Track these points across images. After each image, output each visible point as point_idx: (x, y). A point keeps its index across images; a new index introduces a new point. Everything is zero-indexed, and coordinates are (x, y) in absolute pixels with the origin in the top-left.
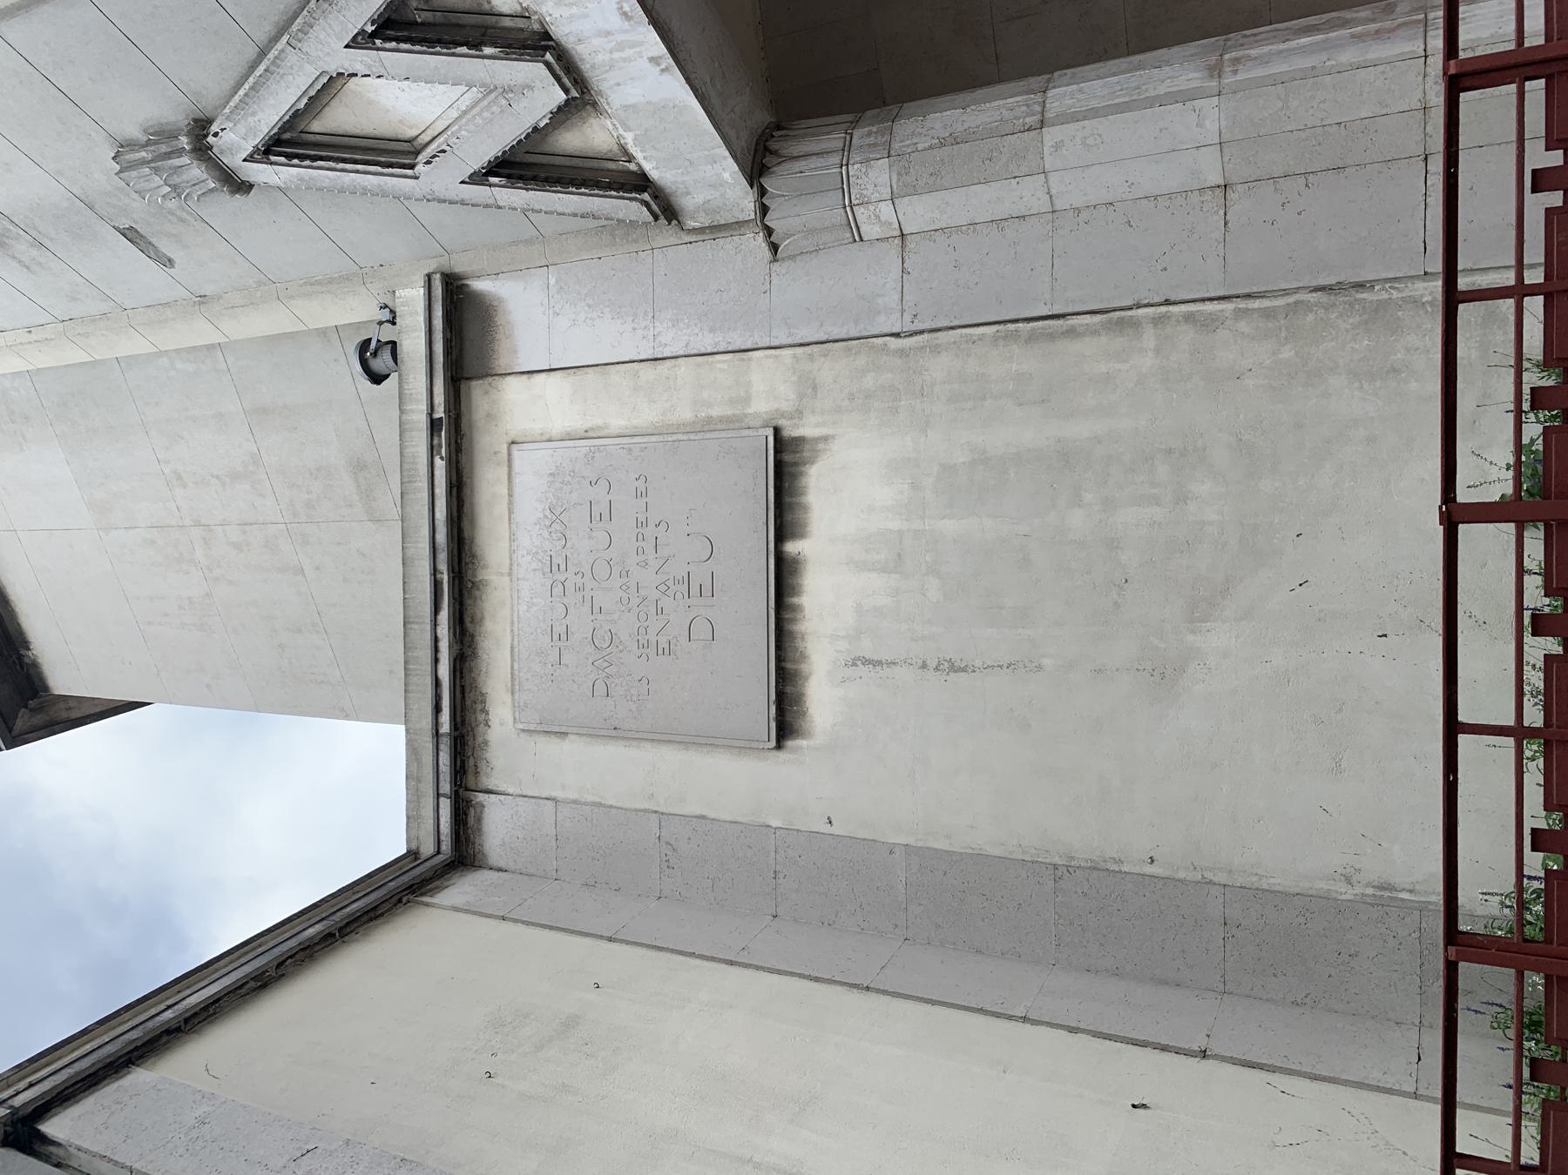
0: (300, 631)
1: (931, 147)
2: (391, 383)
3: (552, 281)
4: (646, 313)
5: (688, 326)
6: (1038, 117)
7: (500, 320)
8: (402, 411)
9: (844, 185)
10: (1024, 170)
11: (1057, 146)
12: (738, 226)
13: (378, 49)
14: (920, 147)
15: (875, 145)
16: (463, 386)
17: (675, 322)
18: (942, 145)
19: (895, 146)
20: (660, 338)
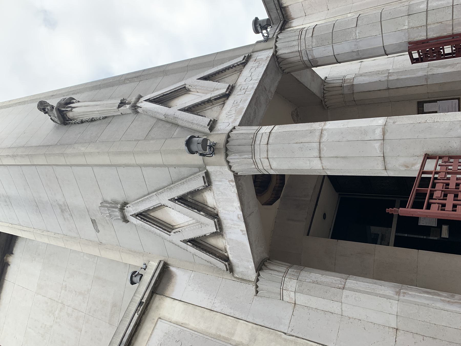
1: (310, 282)
3: (192, 275)
4: (214, 295)
6: (343, 286)
7: (173, 280)
9: (282, 283)
11: (347, 296)
14: (307, 281)
15: (294, 275)
18: (313, 283)
19: (300, 278)
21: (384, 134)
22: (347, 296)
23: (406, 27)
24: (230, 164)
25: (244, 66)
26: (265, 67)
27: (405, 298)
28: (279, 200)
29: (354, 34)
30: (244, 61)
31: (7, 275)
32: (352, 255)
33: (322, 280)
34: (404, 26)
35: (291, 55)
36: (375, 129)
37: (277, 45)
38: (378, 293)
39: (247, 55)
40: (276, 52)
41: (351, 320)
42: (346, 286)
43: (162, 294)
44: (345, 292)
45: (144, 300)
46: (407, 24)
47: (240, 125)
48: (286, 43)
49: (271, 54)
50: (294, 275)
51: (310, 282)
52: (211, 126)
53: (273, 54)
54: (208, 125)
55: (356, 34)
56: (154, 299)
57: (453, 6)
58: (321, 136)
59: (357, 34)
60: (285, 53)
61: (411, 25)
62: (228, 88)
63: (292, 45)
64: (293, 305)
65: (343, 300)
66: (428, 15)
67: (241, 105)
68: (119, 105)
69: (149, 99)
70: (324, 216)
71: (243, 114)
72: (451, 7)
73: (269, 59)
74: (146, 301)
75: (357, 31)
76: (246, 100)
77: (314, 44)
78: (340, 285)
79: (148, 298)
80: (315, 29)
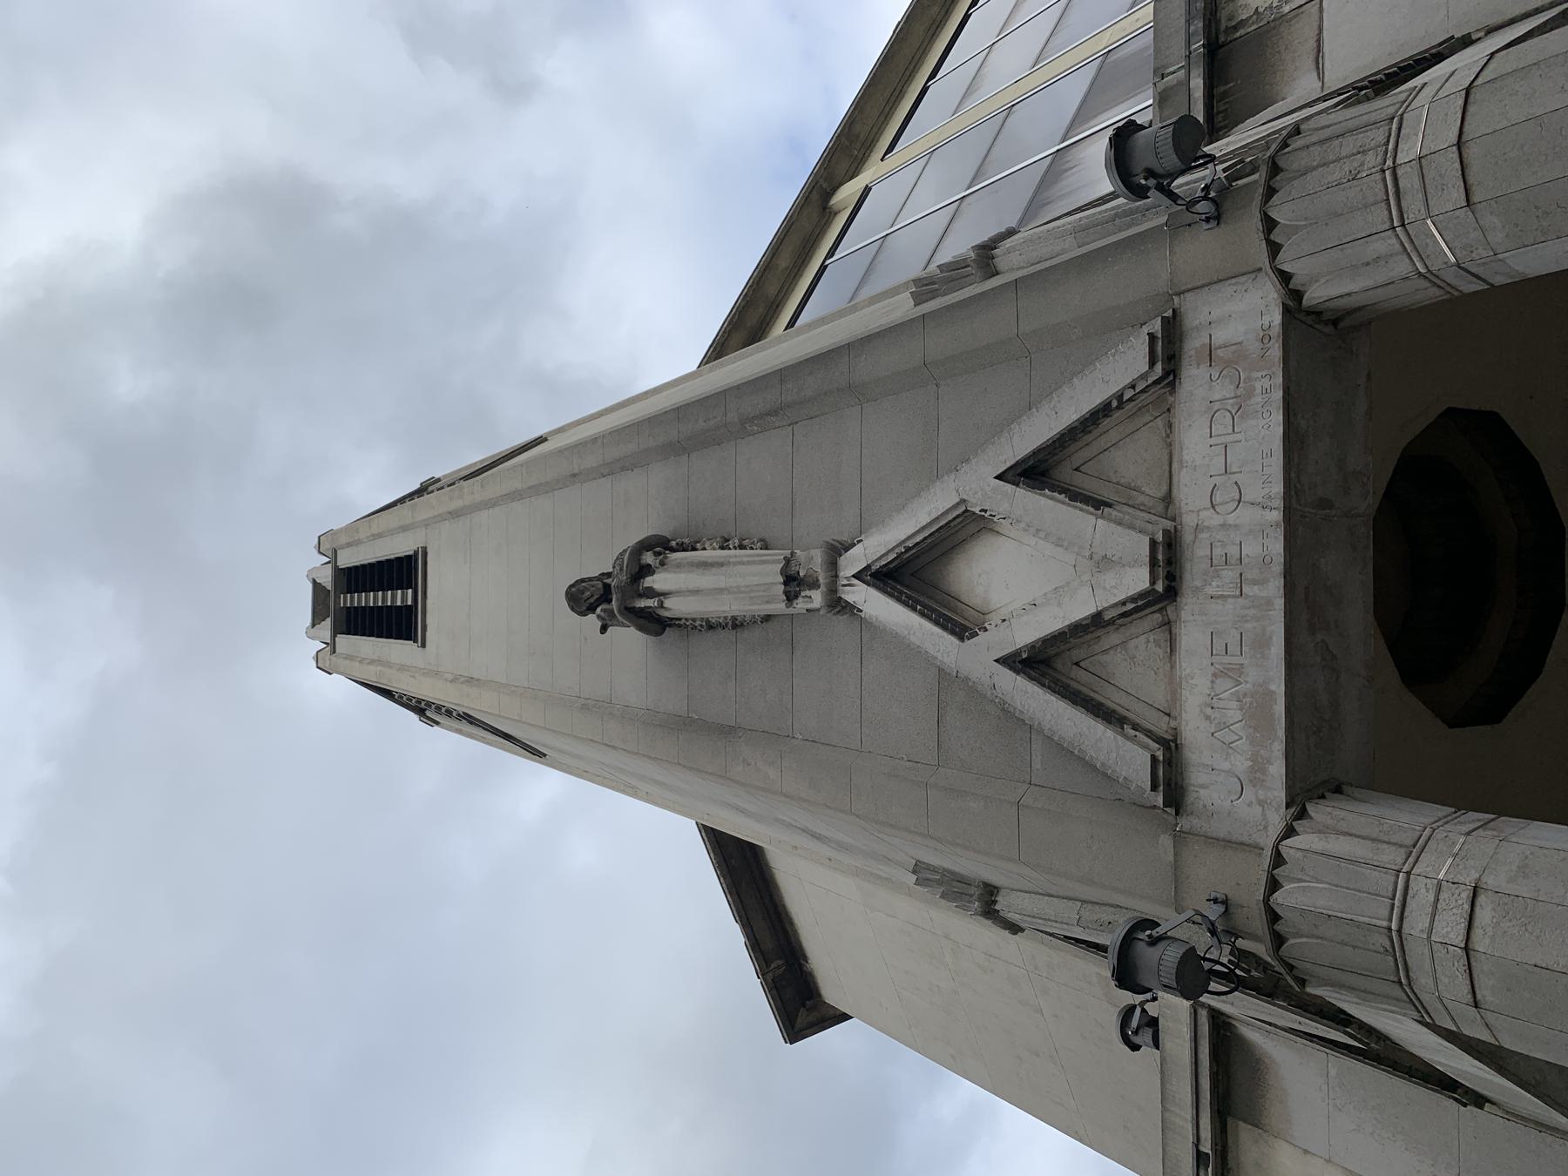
25: (1172, 386)
26: (1279, 417)
30: (1159, 368)
31: (769, 857)
37: (1274, 214)
40: (1297, 295)
45: (1206, 1148)
49: (1277, 318)
52: (1168, 784)
53: (1286, 310)
54: (1154, 788)
67: (1252, 676)
68: (786, 593)
69: (868, 567)
71: (1281, 733)
73: (1276, 351)
74: (1214, 1144)
76: (1262, 643)
77: (1497, 237)
79: (1214, 1137)
80: (1472, 152)
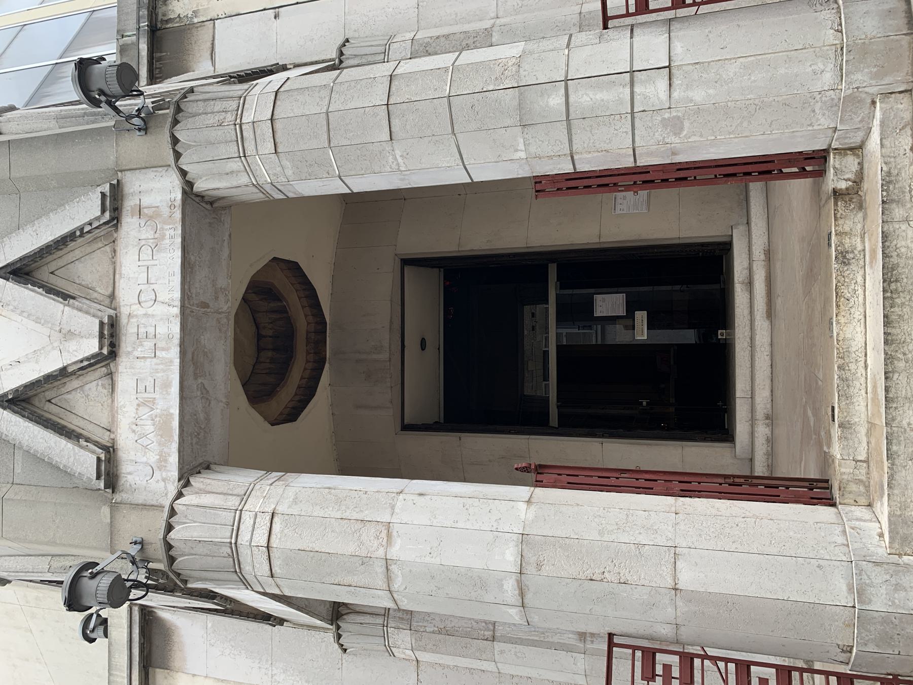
0: (27, 660)
1: (433, 632)
2: (101, 642)
3: (210, 625)
4: (267, 661)
5: (293, 675)
6: (491, 633)
7: (175, 638)
8: (110, 674)
9: (385, 636)
10: (484, 657)
11: (502, 652)
12: (521, 94)
13: (81, 447)
14: (428, 629)
15: (402, 619)
16: (150, 669)
17: (285, 671)
18: (440, 633)
19: (414, 624)
20: (275, 677)
21: (522, 594)
22: (502, 652)
23: (522, 155)
24: (178, 148)
27: (595, 646)
28: (327, 366)
29: (391, 159)
32: (490, 461)
33: (453, 624)
34: (517, 150)
35: (234, 192)
36: (501, 580)
38: (551, 640)
39: (106, 188)
40: (190, 184)
41: (516, 680)
42: (498, 634)
43: (166, 667)
44: (498, 646)
46: (521, 147)
47: (185, 479)
48: (210, 164)
50: (402, 619)
51: (433, 632)
52: (108, 474)
53: (184, 192)
55: (396, 159)
56: (154, 677)
57: (632, 113)
58: (389, 578)
59: (400, 160)
60: (218, 189)
61: (533, 149)
62: (101, 336)
63: (228, 171)
64: (415, 663)
65: (497, 657)
66: (573, 131)
70: (423, 344)
71: (176, 438)
72: (629, 116)
75: (398, 153)
76: (167, 385)
78: (486, 633)
